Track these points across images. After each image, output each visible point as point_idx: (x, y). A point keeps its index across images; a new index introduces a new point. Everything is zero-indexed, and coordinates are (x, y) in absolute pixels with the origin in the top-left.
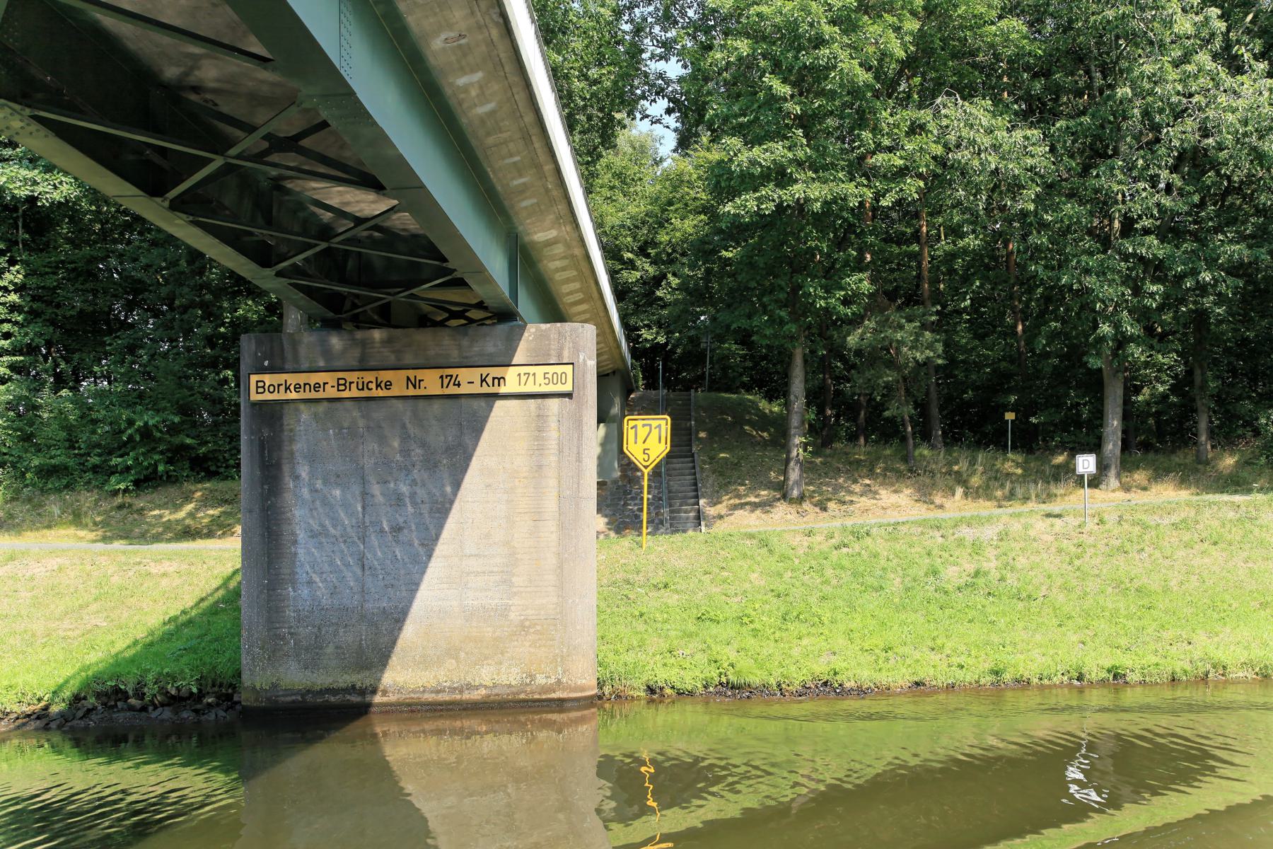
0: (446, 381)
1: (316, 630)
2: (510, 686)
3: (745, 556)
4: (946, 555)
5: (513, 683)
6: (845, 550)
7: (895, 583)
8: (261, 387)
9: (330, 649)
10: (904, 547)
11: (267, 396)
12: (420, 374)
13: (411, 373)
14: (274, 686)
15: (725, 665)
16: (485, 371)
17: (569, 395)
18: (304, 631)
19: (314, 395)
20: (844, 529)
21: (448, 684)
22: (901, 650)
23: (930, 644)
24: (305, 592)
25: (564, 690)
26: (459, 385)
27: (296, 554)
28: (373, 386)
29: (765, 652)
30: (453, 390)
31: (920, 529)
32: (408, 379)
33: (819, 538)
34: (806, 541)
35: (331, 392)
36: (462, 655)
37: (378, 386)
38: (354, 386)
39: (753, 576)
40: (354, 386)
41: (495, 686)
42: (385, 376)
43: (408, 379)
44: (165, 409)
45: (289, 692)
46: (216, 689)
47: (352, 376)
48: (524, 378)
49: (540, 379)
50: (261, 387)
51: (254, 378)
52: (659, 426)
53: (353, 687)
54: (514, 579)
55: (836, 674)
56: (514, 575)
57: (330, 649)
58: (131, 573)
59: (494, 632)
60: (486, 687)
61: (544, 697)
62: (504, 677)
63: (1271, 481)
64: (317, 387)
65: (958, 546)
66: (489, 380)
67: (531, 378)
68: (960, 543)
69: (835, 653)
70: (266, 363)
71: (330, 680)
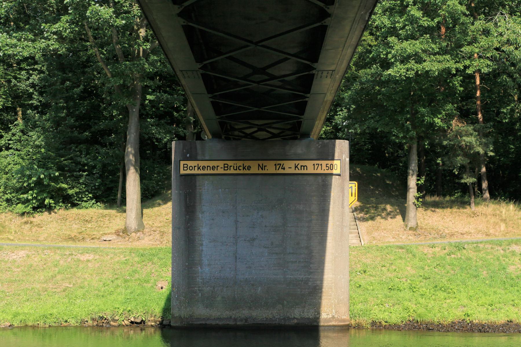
0: (278, 167)
1: (212, 289)
2: (309, 319)
3: (401, 258)
4: (507, 260)
5: (311, 317)
6: (453, 256)
7: (484, 273)
8: (186, 167)
9: (219, 298)
10: (484, 255)
11: (188, 172)
12: (265, 163)
13: (261, 162)
14: (191, 316)
15: (411, 311)
16: (297, 162)
17: (339, 175)
18: (207, 289)
19: (212, 172)
20: (450, 244)
21: (278, 317)
22: (498, 306)
23: (511, 303)
24: (207, 269)
25: (336, 321)
26: (284, 169)
27: (202, 250)
28: (241, 168)
29: (430, 306)
30: (281, 171)
31: (490, 246)
32: (259, 165)
33: (437, 249)
34: (431, 251)
35: (221, 171)
36: (285, 302)
37: (244, 168)
38: (232, 168)
39: (409, 268)
40: (232, 168)
41: (302, 318)
42: (247, 163)
43: (259, 165)
44: (51, 168)
45: (198, 319)
46: (153, 318)
47: (230, 163)
48: (316, 166)
49: (324, 167)
50: (186, 167)
51: (182, 163)
52: (351, 187)
53: (231, 317)
54: (311, 265)
55: (468, 316)
56: (311, 263)
57: (219, 298)
58: (69, 260)
59: (301, 292)
60: (297, 319)
61: (326, 324)
62: (306, 314)
63: (520, 201)
64: (213, 168)
65: (513, 255)
66: (299, 167)
67: (320, 166)
68: (513, 253)
69: (464, 306)
70: (188, 155)
71: (219, 314)
